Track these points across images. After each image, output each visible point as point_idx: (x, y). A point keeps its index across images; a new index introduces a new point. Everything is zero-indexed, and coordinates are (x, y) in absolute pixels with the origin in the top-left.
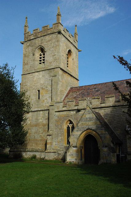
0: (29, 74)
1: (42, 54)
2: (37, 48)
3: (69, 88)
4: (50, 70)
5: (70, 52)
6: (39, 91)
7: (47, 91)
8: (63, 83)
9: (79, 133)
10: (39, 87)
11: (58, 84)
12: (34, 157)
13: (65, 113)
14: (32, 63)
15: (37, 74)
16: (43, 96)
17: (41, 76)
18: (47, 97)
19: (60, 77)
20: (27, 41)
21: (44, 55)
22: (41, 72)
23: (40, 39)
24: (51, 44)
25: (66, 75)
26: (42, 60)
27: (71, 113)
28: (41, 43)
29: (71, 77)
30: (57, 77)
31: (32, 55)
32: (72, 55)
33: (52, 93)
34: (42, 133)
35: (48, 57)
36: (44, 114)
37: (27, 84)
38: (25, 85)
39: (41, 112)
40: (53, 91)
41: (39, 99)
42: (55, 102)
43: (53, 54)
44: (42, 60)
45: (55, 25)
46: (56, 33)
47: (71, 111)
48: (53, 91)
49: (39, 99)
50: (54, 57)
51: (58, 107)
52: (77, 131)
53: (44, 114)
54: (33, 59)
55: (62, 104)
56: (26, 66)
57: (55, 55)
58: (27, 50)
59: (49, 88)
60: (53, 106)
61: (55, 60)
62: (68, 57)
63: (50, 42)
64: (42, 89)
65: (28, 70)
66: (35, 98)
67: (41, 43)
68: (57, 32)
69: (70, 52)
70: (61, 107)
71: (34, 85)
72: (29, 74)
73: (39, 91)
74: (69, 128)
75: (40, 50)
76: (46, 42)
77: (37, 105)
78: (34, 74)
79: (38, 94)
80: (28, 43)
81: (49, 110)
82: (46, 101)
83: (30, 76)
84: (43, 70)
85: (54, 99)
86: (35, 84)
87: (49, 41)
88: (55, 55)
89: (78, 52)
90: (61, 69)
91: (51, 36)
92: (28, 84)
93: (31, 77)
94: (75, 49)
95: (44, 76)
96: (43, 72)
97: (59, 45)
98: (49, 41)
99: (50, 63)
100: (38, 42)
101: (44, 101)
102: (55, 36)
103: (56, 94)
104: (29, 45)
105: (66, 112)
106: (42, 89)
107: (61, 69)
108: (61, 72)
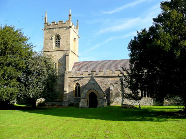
0: (49, 51)
1: (57, 39)
3: (74, 63)
5: (75, 39)
9: (87, 91)
12: (159, 101)
15: (55, 52)
21: (59, 40)
22: (57, 52)
24: (65, 34)
26: (58, 44)
28: (58, 32)
34: (58, 90)
52: (85, 90)
56: (46, 46)
67: (58, 32)
69: (75, 39)
70: (79, 74)
72: (49, 51)
74: (77, 87)
80: (48, 31)
100: (56, 31)
104: (48, 32)
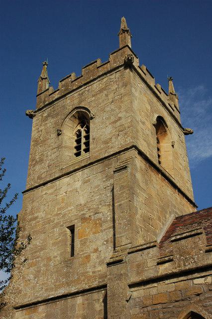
2: (69, 116)
3: (170, 219)
4: (106, 162)
6: (72, 229)
7: (99, 223)
8: (150, 196)
10: (72, 214)
11: (132, 194)
13: (168, 286)
14: (53, 156)
15: (66, 180)
16: (84, 243)
17: (78, 185)
18: (99, 243)
19: (139, 176)
20: (43, 108)
23: (76, 94)
24: (107, 95)
25: (156, 178)
27: (196, 281)
29: (173, 189)
30: (129, 170)
31: (54, 135)
32: (168, 132)
33: (114, 227)
35: (100, 129)
36: (90, 306)
37: (36, 215)
38: (31, 220)
39: (79, 300)
40: (115, 62)
41: (72, 254)
42: (128, 251)
43: (113, 119)
44: (83, 144)
45: (115, 54)
46: (118, 68)
47: (196, 275)
48: (115, 62)
49: (72, 254)
50: (118, 124)
51: (138, 266)
53: (90, 306)
54: (56, 146)
55: (154, 252)
57: (120, 118)
58: (43, 128)
59: (106, 212)
60: (119, 266)
61: (121, 130)
62: (157, 139)
63: (105, 92)
64: (84, 219)
65: (43, 176)
66: (59, 252)
67: (80, 102)
68: (121, 66)
70: (151, 263)
71: (57, 215)
73: (72, 229)
75: (77, 121)
76: (93, 96)
77: (67, 275)
78: (57, 182)
79: (69, 239)
81: (105, 286)
82: (94, 256)
83: (48, 189)
84: (85, 166)
85: (123, 240)
86: (59, 209)
87: (101, 91)
88: (120, 118)
89: (183, 136)
90: (141, 153)
91: (105, 80)
92: (41, 214)
93: (50, 191)
94: (176, 125)
95: (89, 180)
96: (86, 171)
97: (130, 94)
98: (101, 91)
99: (106, 142)
101: (88, 257)
102: (118, 75)
103: (130, 222)
104: (49, 116)
105: (175, 280)
106: (84, 219)
107: (141, 153)
108: (139, 162)
